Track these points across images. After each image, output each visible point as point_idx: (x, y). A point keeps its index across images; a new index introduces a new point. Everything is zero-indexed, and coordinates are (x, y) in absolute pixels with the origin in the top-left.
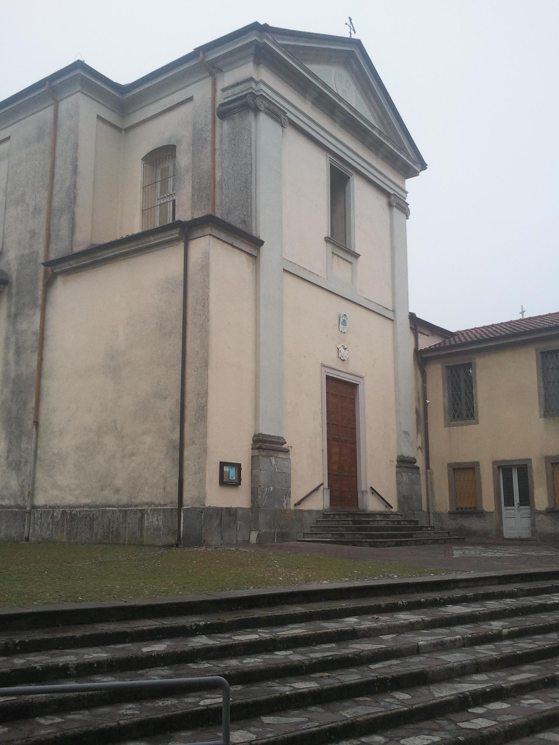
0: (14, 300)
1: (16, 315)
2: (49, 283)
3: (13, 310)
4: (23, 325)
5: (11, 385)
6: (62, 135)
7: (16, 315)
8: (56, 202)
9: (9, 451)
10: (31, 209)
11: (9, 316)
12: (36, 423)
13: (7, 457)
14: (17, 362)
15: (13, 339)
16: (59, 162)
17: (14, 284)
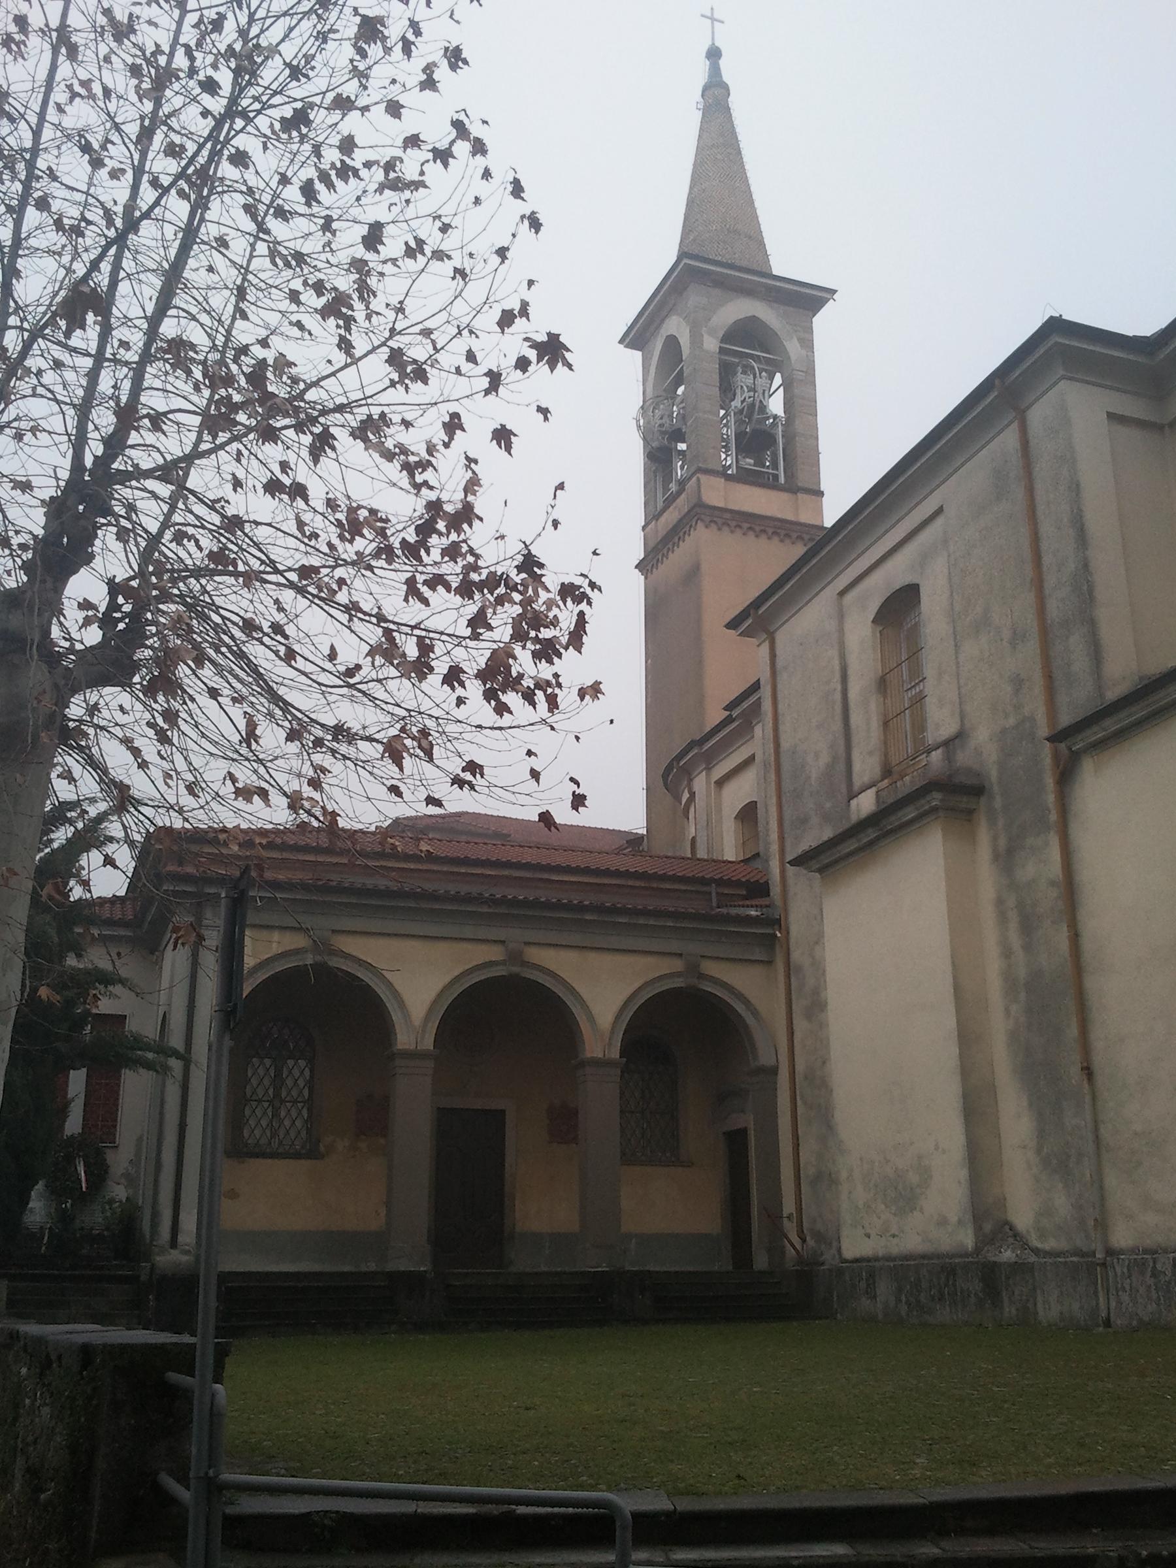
0: (1001, 823)
1: (1010, 852)
2: (1066, 775)
3: (1002, 842)
4: (1028, 870)
5: (1023, 996)
6: (1043, 470)
7: (1010, 852)
8: (1054, 609)
9: (1041, 1134)
10: (1006, 634)
11: (996, 857)
12: (1088, 1071)
13: (1039, 1151)
14: (1028, 948)
15: (1011, 902)
16: (1046, 528)
17: (996, 788)
